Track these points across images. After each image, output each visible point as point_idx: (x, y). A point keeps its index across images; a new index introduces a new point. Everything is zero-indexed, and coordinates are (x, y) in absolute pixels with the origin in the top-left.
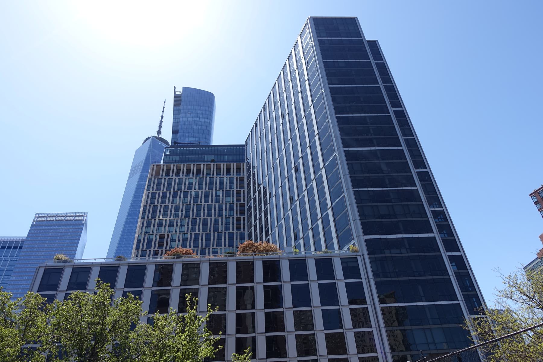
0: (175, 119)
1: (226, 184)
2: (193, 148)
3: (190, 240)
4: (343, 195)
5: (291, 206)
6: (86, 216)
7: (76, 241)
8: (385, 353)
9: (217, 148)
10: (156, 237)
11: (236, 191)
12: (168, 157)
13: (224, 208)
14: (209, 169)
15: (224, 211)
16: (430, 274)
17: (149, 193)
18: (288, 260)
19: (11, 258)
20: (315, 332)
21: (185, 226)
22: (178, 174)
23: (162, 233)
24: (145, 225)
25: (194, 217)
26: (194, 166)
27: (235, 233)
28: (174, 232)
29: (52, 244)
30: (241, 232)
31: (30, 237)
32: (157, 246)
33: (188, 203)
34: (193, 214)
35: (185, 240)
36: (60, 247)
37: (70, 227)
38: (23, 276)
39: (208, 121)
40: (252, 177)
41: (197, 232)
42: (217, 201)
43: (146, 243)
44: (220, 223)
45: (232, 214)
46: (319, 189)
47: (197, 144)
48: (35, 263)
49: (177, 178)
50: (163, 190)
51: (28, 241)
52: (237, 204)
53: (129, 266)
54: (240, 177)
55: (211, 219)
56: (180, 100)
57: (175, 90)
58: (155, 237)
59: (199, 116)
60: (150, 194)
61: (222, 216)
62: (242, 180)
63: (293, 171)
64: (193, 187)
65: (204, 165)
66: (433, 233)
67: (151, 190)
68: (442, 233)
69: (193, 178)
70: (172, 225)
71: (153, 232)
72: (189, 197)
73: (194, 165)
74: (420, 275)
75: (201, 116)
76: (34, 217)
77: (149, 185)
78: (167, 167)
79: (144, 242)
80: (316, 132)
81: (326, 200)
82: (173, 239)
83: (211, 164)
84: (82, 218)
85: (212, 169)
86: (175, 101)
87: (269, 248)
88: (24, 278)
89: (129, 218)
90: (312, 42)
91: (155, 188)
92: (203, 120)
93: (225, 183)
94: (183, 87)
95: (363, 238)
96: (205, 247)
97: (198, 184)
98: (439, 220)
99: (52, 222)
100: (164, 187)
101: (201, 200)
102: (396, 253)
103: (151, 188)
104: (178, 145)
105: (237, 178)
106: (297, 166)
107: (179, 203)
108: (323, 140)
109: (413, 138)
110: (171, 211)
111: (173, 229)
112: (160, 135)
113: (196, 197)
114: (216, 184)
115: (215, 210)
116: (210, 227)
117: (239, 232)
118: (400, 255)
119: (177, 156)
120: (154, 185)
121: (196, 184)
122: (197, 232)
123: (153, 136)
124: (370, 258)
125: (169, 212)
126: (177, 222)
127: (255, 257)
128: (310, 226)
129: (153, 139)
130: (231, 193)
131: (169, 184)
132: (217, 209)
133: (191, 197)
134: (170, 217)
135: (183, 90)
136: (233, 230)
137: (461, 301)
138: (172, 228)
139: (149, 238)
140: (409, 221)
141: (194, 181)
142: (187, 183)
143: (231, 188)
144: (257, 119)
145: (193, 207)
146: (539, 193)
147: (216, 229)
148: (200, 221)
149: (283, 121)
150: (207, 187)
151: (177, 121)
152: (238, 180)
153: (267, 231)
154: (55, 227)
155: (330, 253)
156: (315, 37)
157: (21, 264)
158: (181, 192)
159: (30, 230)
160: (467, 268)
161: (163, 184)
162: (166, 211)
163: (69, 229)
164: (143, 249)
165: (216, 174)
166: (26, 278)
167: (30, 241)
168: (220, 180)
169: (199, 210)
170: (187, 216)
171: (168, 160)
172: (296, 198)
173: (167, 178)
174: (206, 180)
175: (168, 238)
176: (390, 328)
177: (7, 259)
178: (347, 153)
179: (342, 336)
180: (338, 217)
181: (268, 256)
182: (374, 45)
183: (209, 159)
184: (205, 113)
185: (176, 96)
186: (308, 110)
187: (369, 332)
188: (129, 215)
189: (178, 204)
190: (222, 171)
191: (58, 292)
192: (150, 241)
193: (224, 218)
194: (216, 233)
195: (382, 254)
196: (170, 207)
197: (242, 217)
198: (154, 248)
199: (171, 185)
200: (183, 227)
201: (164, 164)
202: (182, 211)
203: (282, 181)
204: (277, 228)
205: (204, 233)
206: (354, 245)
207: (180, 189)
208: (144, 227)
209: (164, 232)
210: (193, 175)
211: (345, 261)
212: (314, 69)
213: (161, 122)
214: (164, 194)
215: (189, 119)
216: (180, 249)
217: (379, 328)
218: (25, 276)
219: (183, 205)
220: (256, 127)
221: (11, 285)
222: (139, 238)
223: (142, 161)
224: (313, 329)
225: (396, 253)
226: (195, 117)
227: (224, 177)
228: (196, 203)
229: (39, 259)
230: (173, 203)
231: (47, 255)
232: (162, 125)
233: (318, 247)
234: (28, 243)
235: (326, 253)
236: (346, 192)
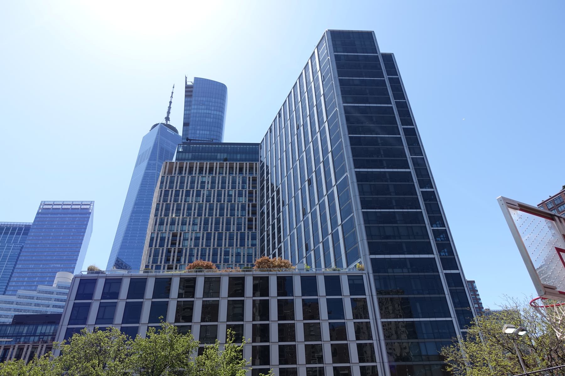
1: (239, 183)
3: (203, 240)
5: (303, 218)
6: (93, 205)
7: (83, 230)
9: (230, 146)
12: (181, 154)
13: (236, 208)
14: (221, 167)
15: (236, 211)
16: (428, 292)
18: (300, 277)
19: (14, 244)
20: (321, 321)
21: (197, 225)
22: (190, 172)
23: (175, 231)
24: (158, 223)
25: (207, 216)
26: (207, 165)
27: (246, 233)
28: (187, 231)
29: (58, 233)
31: (36, 225)
32: (170, 244)
33: (201, 202)
35: (197, 239)
36: (66, 236)
37: (77, 216)
38: (30, 264)
39: (220, 113)
40: (265, 182)
41: (209, 231)
43: (159, 241)
44: (232, 223)
46: (331, 205)
48: (41, 252)
49: (190, 177)
50: (176, 188)
51: (34, 229)
52: (249, 204)
53: (156, 278)
54: (252, 177)
55: (223, 218)
56: (192, 91)
57: (186, 80)
58: (168, 236)
60: (163, 192)
61: (234, 215)
62: (254, 180)
63: (307, 183)
65: (217, 163)
66: (433, 254)
67: (164, 188)
69: (206, 177)
70: (184, 224)
71: (166, 231)
72: (202, 196)
73: (207, 163)
74: (419, 293)
75: (213, 108)
76: (40, 204)
77: (162, 183)
78: (179, 164)
79: (157, 240)
80: (330, 149)
81: (336, 216)
83: (224, 163)
84: (89, 207)
85: (225, 168)
86: (186, 92)
87: (283, 264)
88: (31, 266)
89: (136, 207)
91: (168, 186)
92: (215, 112)
93: (237, 182)
97: (211, 183)
98: (441, 239)
99: (58, 210)
100: (176, 185)
101: (214, 199)
102: (398, 272)
104: (190, 142)
105: (249, 178)
106: (310, 179)
107: (192, 202)
108: (336, 158)
109: (422, 157)
110: (184, 210)
111: (186, 228)
113: (209, 196)
114: (229, 183)
115: (227, 210)
116: (222, 227)
117: (250, 232)
118: (402, 274)
120: (166, 183)
121: (208, 182)
122: (209, 231)
124: (374, 276)
125: (182, 211)
126: (190, 221)
127: (270, 273)
128: (321, 240)
129: (161, 126)
130: (244, 192)
131: (182, 183)
132: (229, 208)
133: (203, 196)
134: (183, 216)
136: (245, 230)
137: (454, 318)
138: (184, 226)
139: (162, 236)
141: (207, 179)
142: (200, 182)
143: (243, 188)
145: (206, 207)
146: (547, 204)
147: (228, 229)
149: (298, 131)
150: (220, 186)
151: (188, 113)
152: (251, 180)
153: (279, 238)
154: (61, 216)
155: (339, 270)
156: (331, 52)
157: (27, 252)
158: (193, 191)
159: (36, 218)
161: (175, 182)
163: (76, 218)
164: (156, 247)
165: (229, 173)
166: (32, 266)
167: (36, 228)
169: (211, 209)
170: (200, 215)
171: (180, 157)
173: (180, 176)
174: (218, 179)
175: (180, 236)
177: (10, 245)
179: (346, 347)
180: (347, 235)
181: (281, 272)
182: (389, 59)
183: (222, 157)
184: (217, 105)
185: (187, 87)
186: (322, 126)
188: (136, 204)
189: (190, 202)
191: (93, 301)
192: (163, 239)
193: (236, 218)
194: (228, 232)
195: (385, 272)
196: (182, 206)
197: (254, 218)
198: (167, 246)
199: (184, 183)
200: (195, 226)
201: (177, 161)
202: (195, 210)
204: (289, 237)
205: (217, 233)
206: (360, 263)
207: (192, 187)
208: (157, 225)
209: (177, 230)
211: (351, 278)
212: (329, 85)
213: (170, 108)
215: (200, 111)
216: (200, 262)
217: (379, 340)
218: (31, 264)
219: (195, 204)
220: (271, 132)
221: (18, 273)
222: (152, 236)
223: (150, 148)
225: (398, 272)
226: (207, 109)
227: (236, 177)
228: (208, 202)
229: (45, 248)
230: (185, 201)
231: (53, 244)
232: (171, 111)
233: (328, 264)
234: (34, 230)
235: (334, 270)
236: (355, 212)
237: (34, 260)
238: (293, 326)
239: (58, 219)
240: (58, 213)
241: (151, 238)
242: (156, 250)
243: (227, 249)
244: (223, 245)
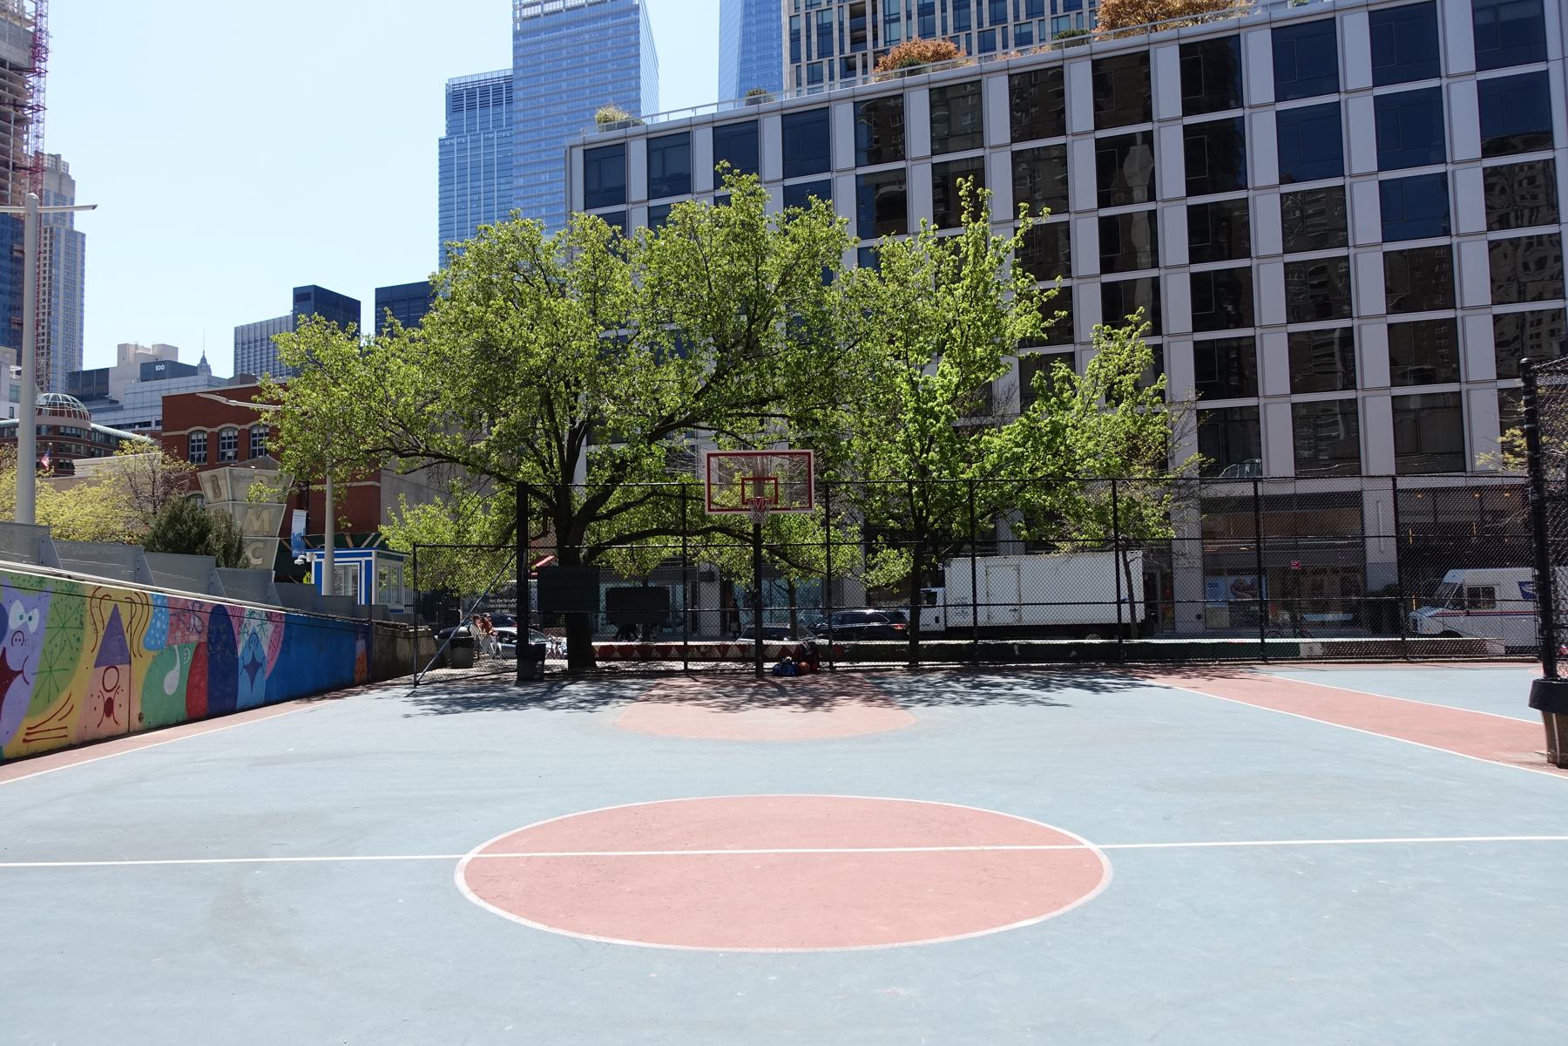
3: (944, 10)
53: (783, 116)
76: (512, 9)
79: (809, 37)
127: (1155, 36)
139: (820, 22)
159: (515, 48)
163: (606, 29)
177: (490, 136)
192: (825, 31)
198: (842, 51)
237: (546, 162)
238: (1253, 415)
239: (565, 41)
240: (560, 25)
241: (791, 34)
242: (811, 67)
243: (1025, 29)
244: (1010, 17)
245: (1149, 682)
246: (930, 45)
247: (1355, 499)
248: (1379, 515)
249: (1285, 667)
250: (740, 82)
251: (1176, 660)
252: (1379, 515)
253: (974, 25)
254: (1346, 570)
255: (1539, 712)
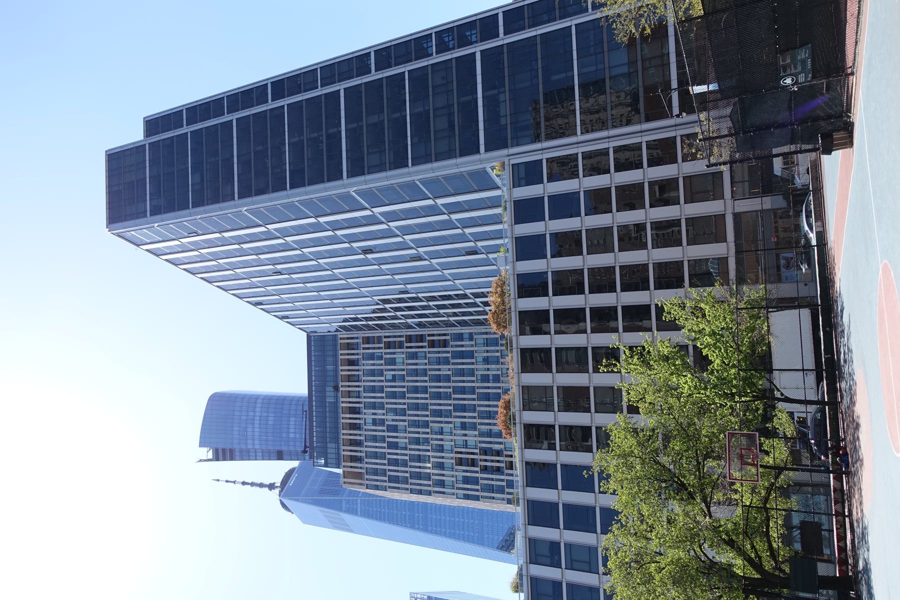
0: (258, 457)
1: (374, 365)
2: (313, 422)
3: (465, 417)
4: (417, 181)
5: (426, 259)
6: (416, 595)
8: (641, 132)
9: (313, 382)
10: (460, 471)
11: (385, 349)
12: (329, 461)
13: (414, 367)
14: (349, 394)
15: (418, 367)
16: (534, 62)
17: (389, 487)
21: (442, 428)
23: (454, 461)
24: (441, 490)
26: (345, 418)
27: (452, 349)
28: (453, 443)
30: (451, 339)
33: (406, 424)
34: (423, 416)
39: (259, 401)
40: (370, 323)
42: (403, 378)
43: (469, 486)
44: (437, 373)
45: (423, 354)
46: (404, 217)
47: (306, 414)
49: (365, 444)
50: (385, 464)
52: (407, 347)
53: (527, 486)
54: (363, 344)
55: (431, 387)
57: (205, 460)
58: (461, 472)
59: (252, 417)
62: (367, 340)
63: (370, 256)
64: (379, 417)
65: (342, 402)
68: (469, 37)
70: (441, 448)
71: (453, 476)
73: (343, 418)
74: (537, 77)
75: (252, 414)
77: (377, 488)
79: (468, 489)
81: (421, 208)
82: (462, 444)
85: (350, 389)
86: (224, 459)
90: (155, 226)
94: (200, 446)
95: (483, 154)
96: (474, 394)
100: (380, 464)
101: (400, 404)
102: (505, 109)
103: (382, 484)
105: (364, 349)
106: (362, 251)
107: (406, 438)
110: (419, 450)
111: (447, 445)
112: (276, 485)
113: (395, 412)
115: (417, 381)
116: (444, 387)
117: (451, 343)
118: (508, 102)
119: (328, 446)
121: (374, 414)
122: (451, 408)
123: (278, 496)
124: (512, 146)
125: (421, 453)
126: (437, 440)
127: (513, 309)
130: (388, 356)
131: (376, 455)
132: (415, 378)
133: (397, 420)
134: (428, 451)
135: (205, 446)
136: (448, 352)
138: (445, 448)
139: (462, 482)
140: (457, 87)
141: (369, 416)
142: (373, 428)
143: (381, 358)
144: (275, 316)
145: (413, 416)
147: (447, 379)
148: (434, 404)
150: (379, 395)
152: (367, 346)
153: (458, 296)
155: (506, 202)
156: (147, 221)
160: (522, 6)
161: (374, 466)
162: (419, 459)
165: (358, 381)
168: (368, 375)
169: (417, 407)
170: (426, 425)
171: (334, 461)
172: (413, 251)
173: (366, 460)
174: (367, 398)
175: (461, 453)
176: (610, 122)
178: (352, 174)
181: (512, 292)
182: (153, 125)
183: (332, 394)
184: (246, 408)
185: (216, 458)
186: (273, 234)
187: (615, 152)
188: (413, 527)
189: (407, 441)
190: (353, 373)
192: (466, 480)
195: (506, 129)
196: (413, 452)
197: (428, 338)
198: (477, 472)
200: (444, 430)
202: (419, 433)
203: (383, 273)
205: (453, 396)
206: (493, 168)
207: (383, 439)
209: (452, 458)
210: (359, 419)
213: (252, 484)
214: (392, 462)
215: (257, 434)
216: (500, 419)
219: (409, 432)
223: (321, 511)
224: (580, 231)
225: (505, 109)
226: (253, 424)
230: (406, 449)
232: (259, 482)
233: (496, 219)
235: (505, 209)
241: (465, 499)
243: (479, 378)
244: (473, 385)
245: (838, 289)
246: (501, 410)
247: (737, 216)
248: (745, 205)
249: (828, 236)
250: (474, 543)
251: (827, 282)
252: (745, 205)
253: (474, 403)
254: (775, 217)
255: (833, 153)
